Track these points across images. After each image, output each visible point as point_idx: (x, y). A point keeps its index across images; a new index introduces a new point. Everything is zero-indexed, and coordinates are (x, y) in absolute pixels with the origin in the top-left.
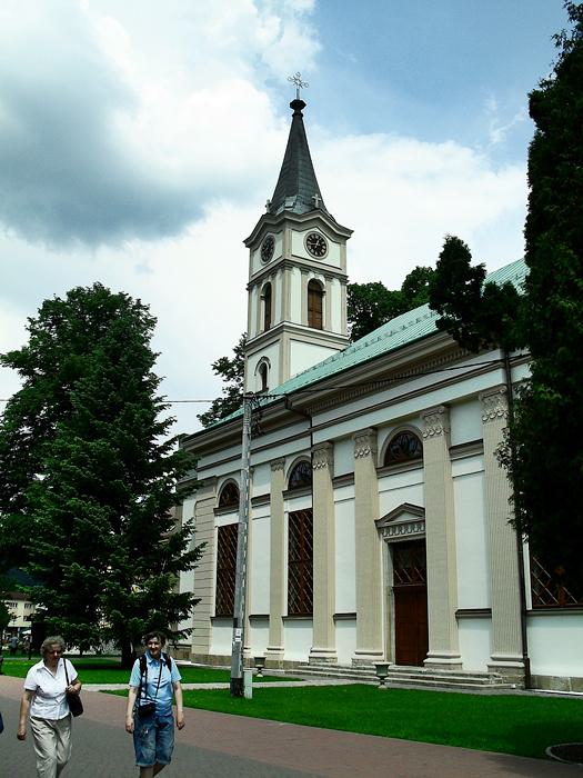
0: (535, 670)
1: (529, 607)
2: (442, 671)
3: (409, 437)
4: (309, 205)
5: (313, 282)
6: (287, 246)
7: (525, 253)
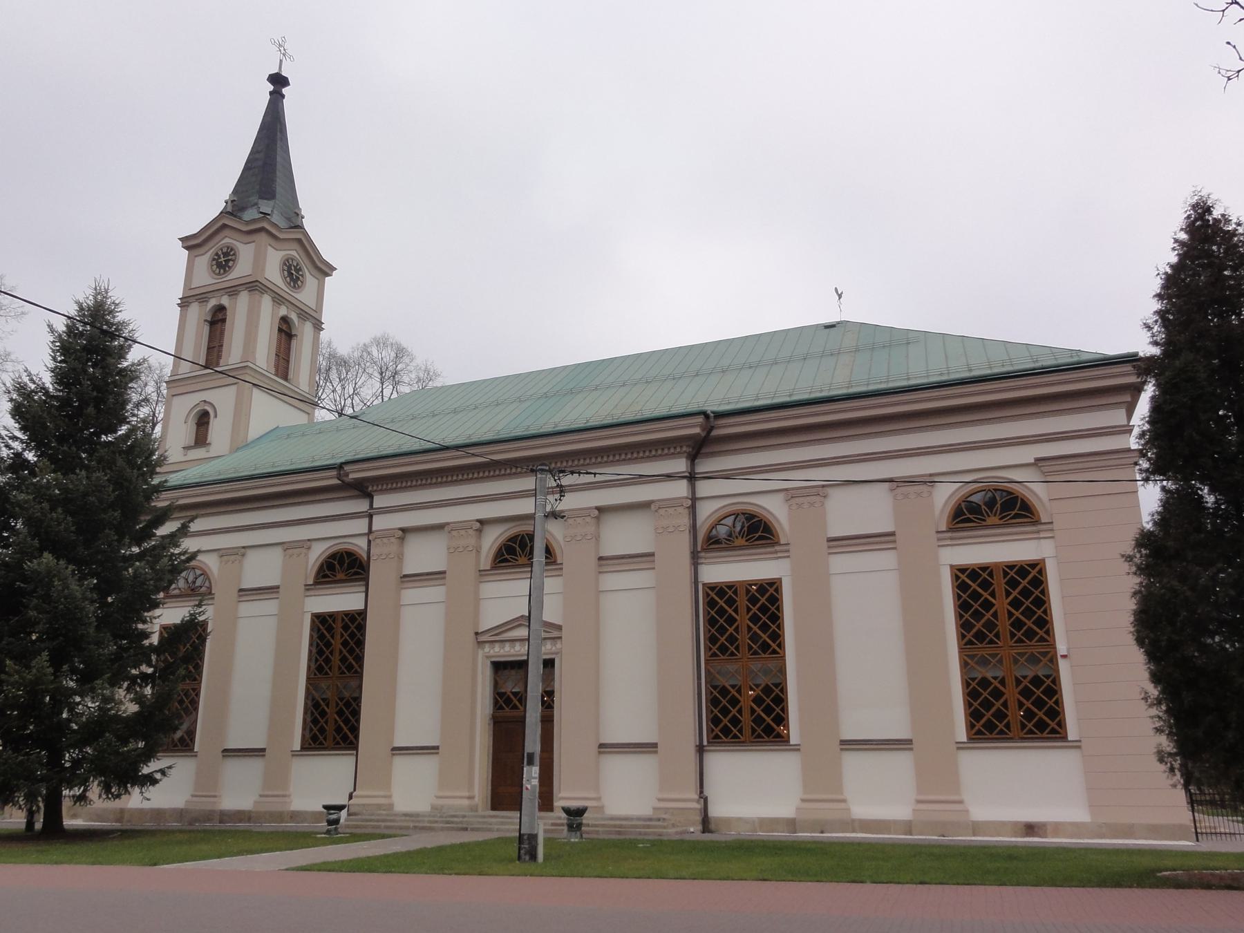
0: (716, 811)
1: (705, 743)
2: (494, 820)
3: (199, 572)
4: (289, 219)
5: (284, 320)
6: (259, 261)
7: (1157, 305)
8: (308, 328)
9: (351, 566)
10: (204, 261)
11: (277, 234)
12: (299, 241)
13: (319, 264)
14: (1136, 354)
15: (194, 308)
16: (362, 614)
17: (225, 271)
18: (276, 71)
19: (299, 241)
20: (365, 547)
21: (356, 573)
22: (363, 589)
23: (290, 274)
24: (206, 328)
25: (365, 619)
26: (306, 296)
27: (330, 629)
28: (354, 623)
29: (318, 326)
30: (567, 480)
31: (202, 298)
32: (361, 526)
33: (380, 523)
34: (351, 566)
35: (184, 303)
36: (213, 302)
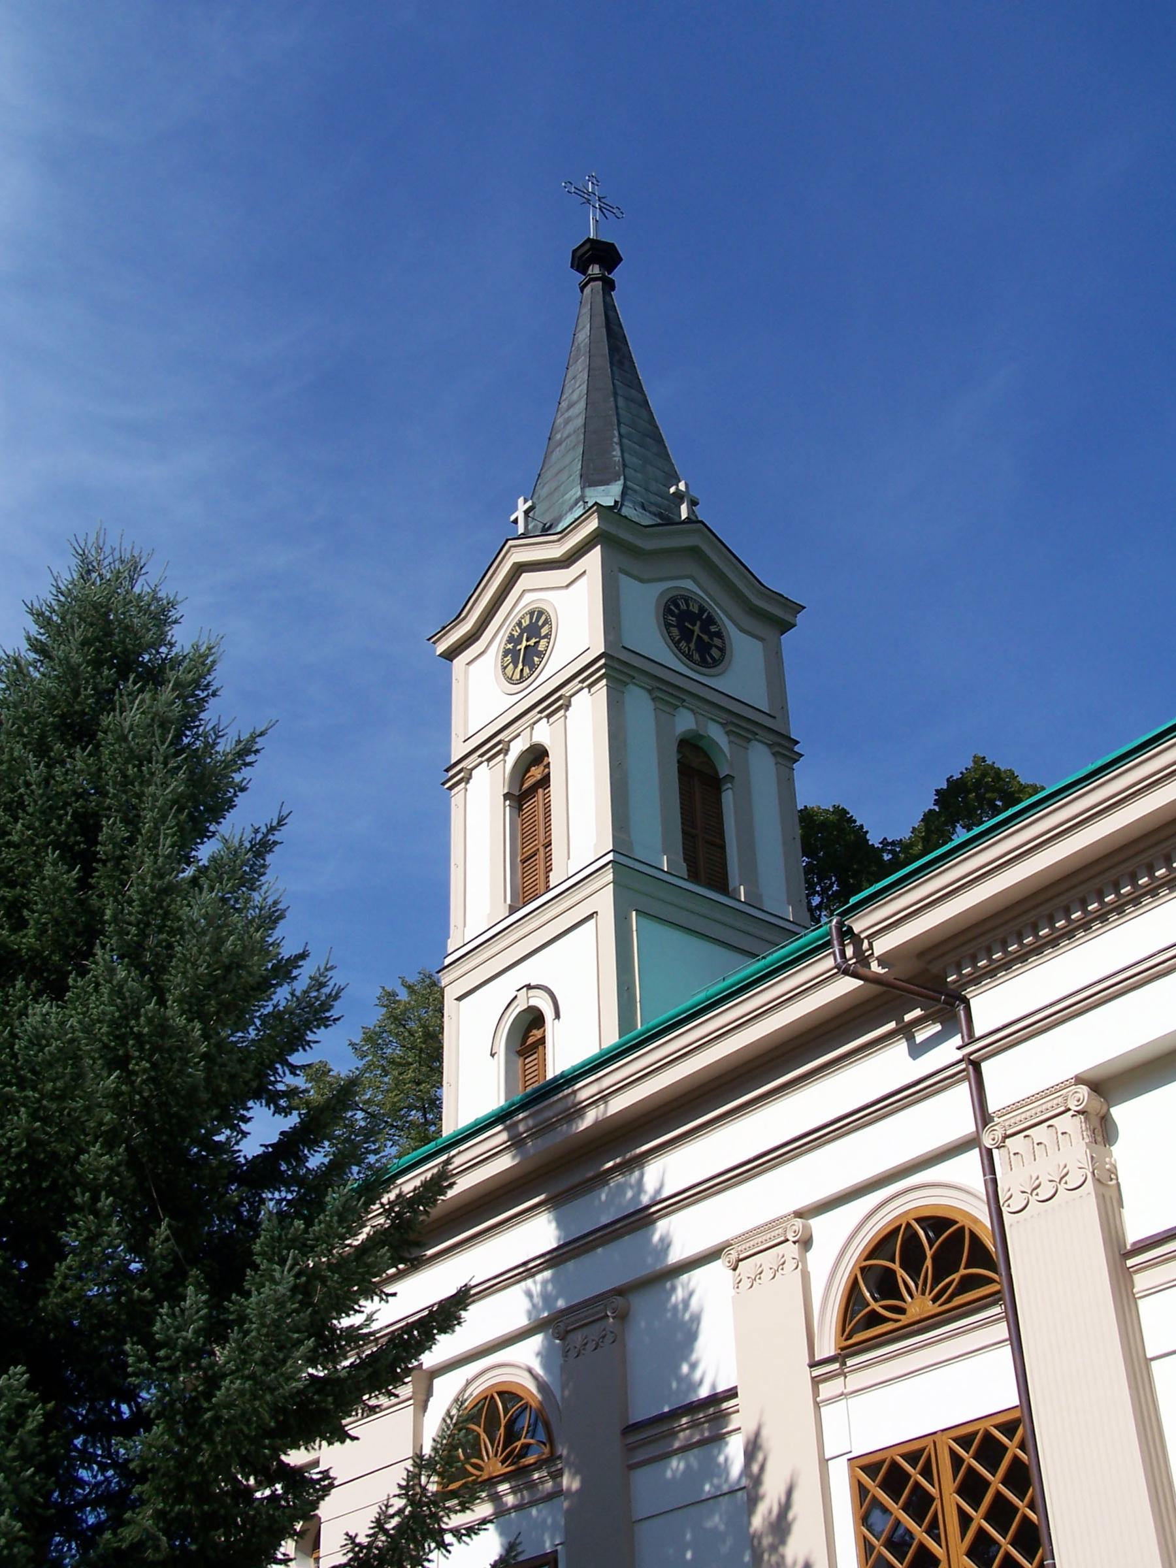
8: (760, 762)
9: (945, 1263)
11: (639, 543)
12: (695, 552)
16: (1017, 1423)
17: (533, 667)
19: (695, 552)
20: (977, 1183)
21: (968, 1283)
22: (1001, 1330)
23: (687, 635)
25: (1029, 1444)
26: (742, 676)
27: (920, 1504)
28: (996, 1465)
29: (786, 750)
32: (951, 1114)
33: (1008, 1079)
34: (945, 1263)
36: (518, 747)
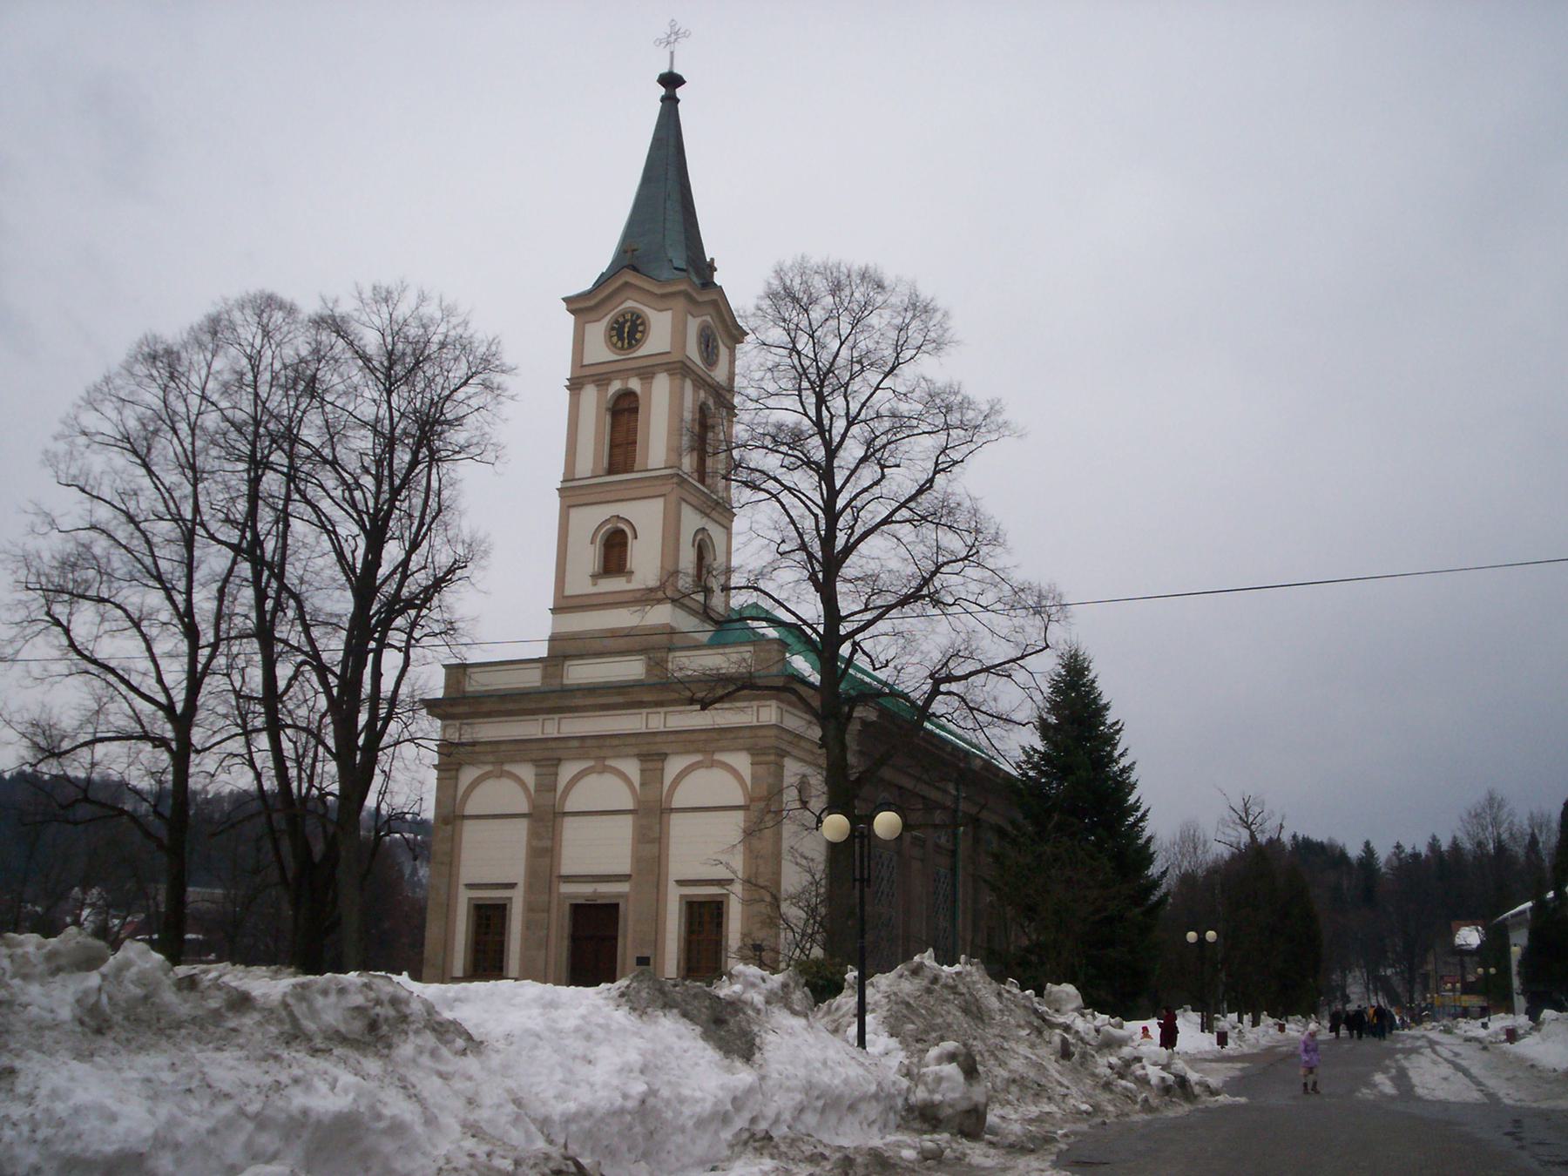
10: (597, 331)
13: (592, 303)
14: (711, 268)
15: (590, 394)
18: (666, 70)
19: (714, 303)
24: (608, 419)
30: (721, 559)
31: (601, 380)
35: (575, 385)
36: (616, 386)
